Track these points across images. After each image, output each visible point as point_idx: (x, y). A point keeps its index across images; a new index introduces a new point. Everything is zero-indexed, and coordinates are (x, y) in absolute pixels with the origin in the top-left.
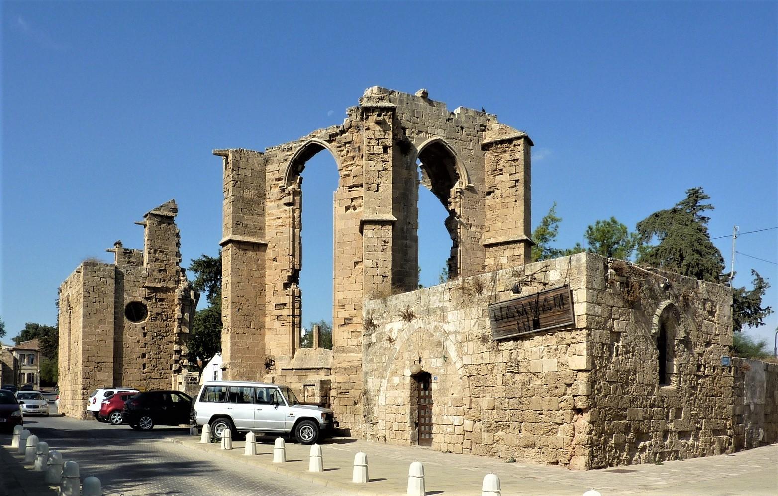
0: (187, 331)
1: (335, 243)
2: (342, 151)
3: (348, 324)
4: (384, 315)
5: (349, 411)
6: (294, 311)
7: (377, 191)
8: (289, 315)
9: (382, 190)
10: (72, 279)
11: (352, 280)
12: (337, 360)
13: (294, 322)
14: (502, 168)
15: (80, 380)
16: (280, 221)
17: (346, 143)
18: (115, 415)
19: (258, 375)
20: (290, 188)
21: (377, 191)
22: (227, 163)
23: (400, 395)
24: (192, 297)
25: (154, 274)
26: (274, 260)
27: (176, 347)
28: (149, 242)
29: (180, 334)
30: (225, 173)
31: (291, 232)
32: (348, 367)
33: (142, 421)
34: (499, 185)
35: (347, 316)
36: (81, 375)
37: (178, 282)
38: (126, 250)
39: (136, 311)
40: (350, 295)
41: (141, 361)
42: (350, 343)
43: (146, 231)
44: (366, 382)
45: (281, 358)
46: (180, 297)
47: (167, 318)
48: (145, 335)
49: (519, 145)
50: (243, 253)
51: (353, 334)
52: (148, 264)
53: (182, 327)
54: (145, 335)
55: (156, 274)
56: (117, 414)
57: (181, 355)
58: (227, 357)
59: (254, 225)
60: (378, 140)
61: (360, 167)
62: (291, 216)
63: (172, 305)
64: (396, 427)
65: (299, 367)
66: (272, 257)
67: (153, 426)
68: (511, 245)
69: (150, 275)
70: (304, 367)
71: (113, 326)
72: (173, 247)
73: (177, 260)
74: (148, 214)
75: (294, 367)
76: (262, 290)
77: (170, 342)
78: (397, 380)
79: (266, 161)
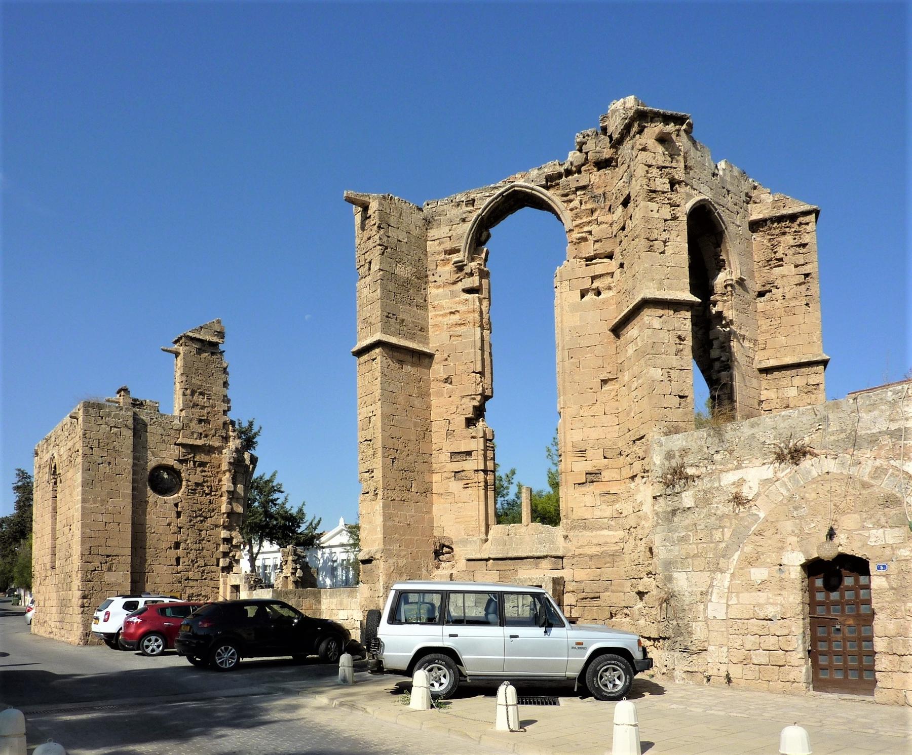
0: (240, 510)
1: (563, 349)
2: (571, 201)
3: (593, 482)
4: (717, 457)
6: (485, 465)
7: (663, 252)
8: (477, 471)
9: (671, 251)
10: (60, 432)
11: (598, 409)
12: (574, 542)
13: (486, 482)
14: (782, 256)
15: (77, 582)
16: (455, 318)
17: (578, 189)
18: (150, 641)
19: (424, 571)
20: (473, 265)
22: (365, 218)
23: (771, 601)
24: (248, 462)
25: (191, 425)
26: (448, 380)
27: (224, 534)
28: (184, 378)
29: (231, 514)
30: (359, 236)
31: (479, 335)
32: (597, 555)
33: (219, 654)
34: (778, 281)
35: (590, 469)
36: (80, 575)
37: (226, 439)
38: (135, 400)
39: (162, 481)
40: (594, 434)
41: (173, 553)
42: (598, 513)
43: (180, 362)
45: (465, 542)
46: (232, 460)
47: (211, 491)
48: (179, 514)
49: (807, 224)
50: (398, 366)
51: (603, 498)
52: (181, 410)
53: (234, 504)
54: (179, 514)
55: (194, 426)
56: (153, 638)
57: (232, 546)
58: (374, 541)
59: (413, 322)
60: (661, 168)
61: (606, 226)
62: (478, 310)
63: (218, 473)
64: (760, 657)
65: (500, 556)
66: (443, 376)
67: (238, 659)
68: (803, 370)
69: (185, 427)
70: (510, 555)
71: (130, 500)
72: (218, 388)
73: (225, 406)
74: (181, 338)
75: (491, 556)
76: (426, 430)
77: (217, 526)
79: (428, 223)
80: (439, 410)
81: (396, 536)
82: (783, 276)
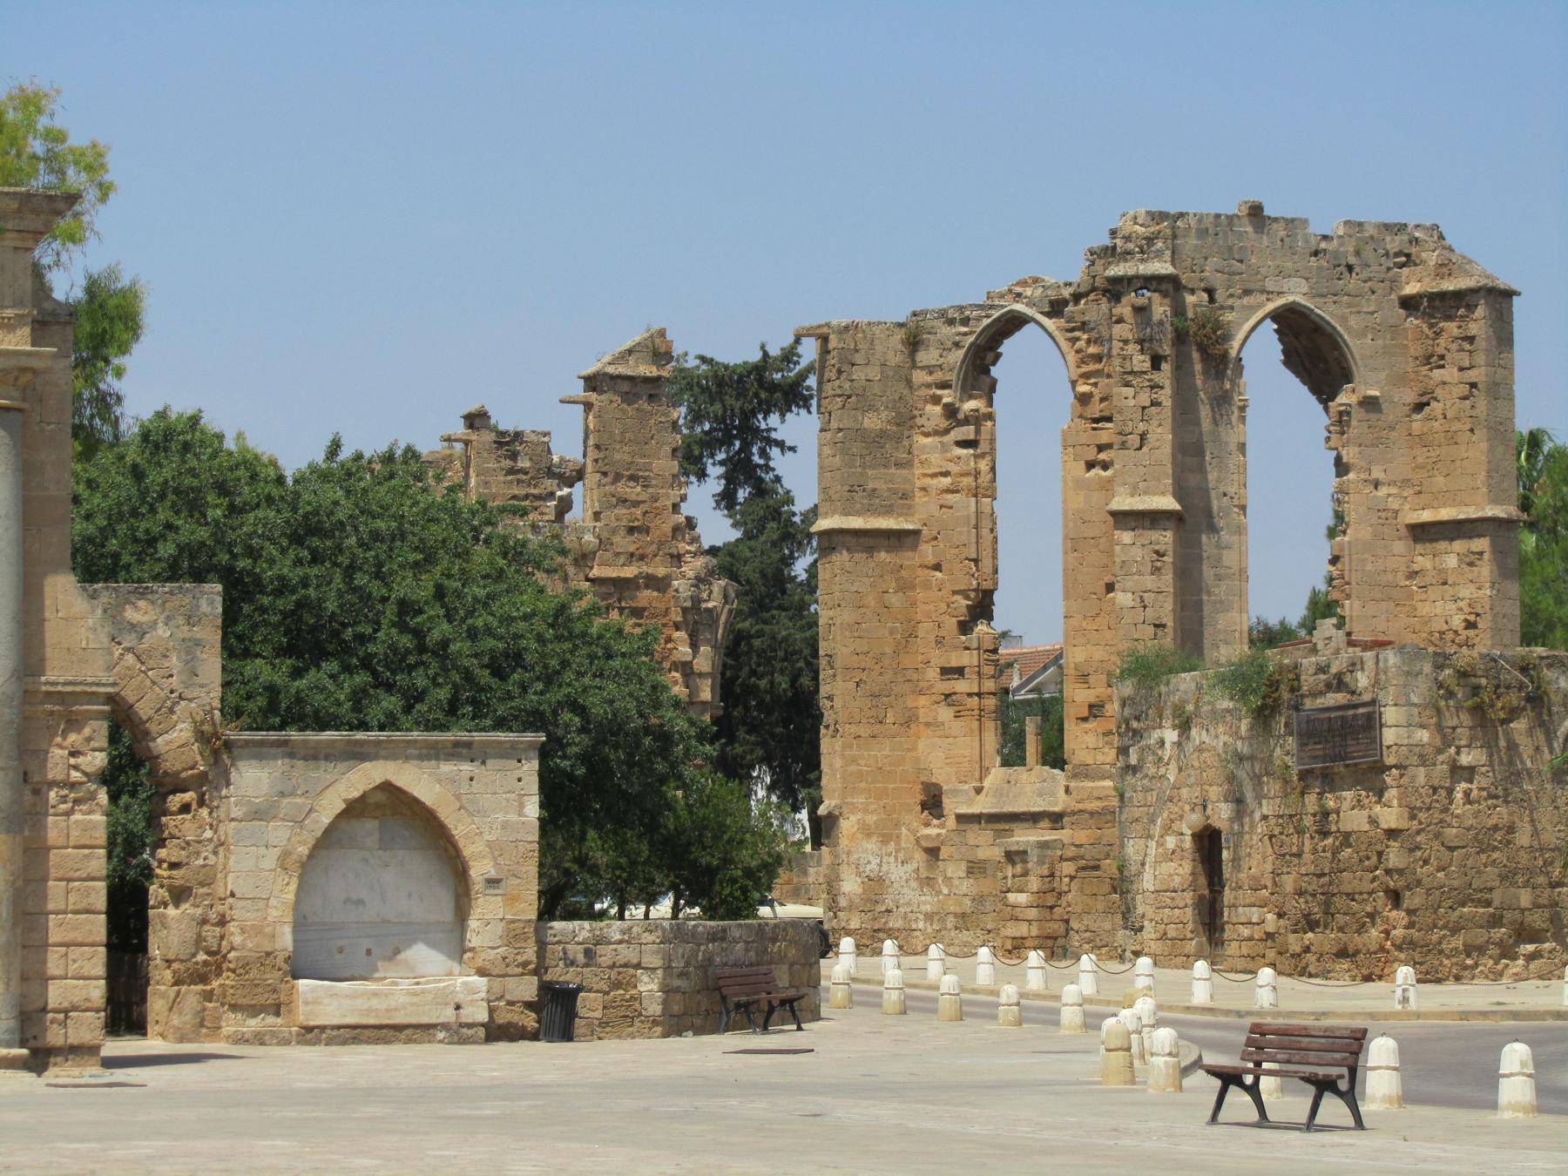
2: (1078, 339)
5: (1100, 906)
16: (947, 481)
21: (1140, 448)
35: (1092, 700)
42: (1100, 758)
44: (1122, 846)
50: (865, 555)
55: (624, 543)
78: (1171, 842)
80: (927, 607)
81: (863, 785)
82: (1444, 383)
